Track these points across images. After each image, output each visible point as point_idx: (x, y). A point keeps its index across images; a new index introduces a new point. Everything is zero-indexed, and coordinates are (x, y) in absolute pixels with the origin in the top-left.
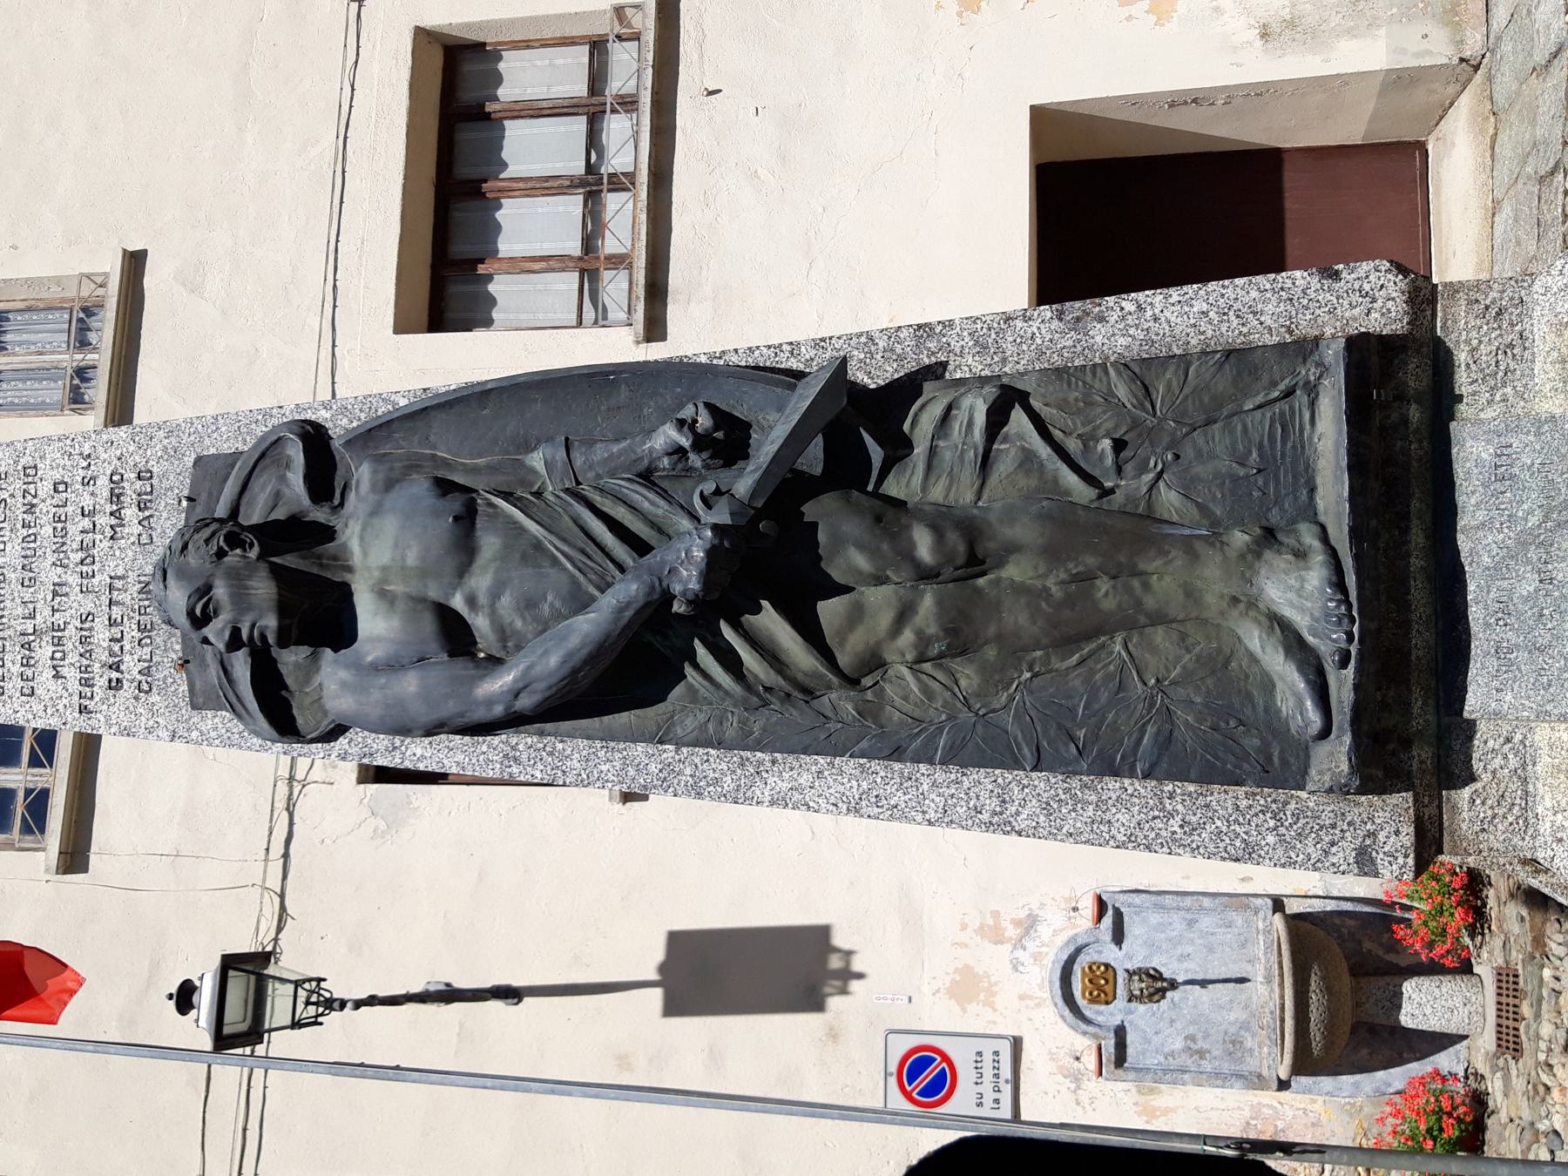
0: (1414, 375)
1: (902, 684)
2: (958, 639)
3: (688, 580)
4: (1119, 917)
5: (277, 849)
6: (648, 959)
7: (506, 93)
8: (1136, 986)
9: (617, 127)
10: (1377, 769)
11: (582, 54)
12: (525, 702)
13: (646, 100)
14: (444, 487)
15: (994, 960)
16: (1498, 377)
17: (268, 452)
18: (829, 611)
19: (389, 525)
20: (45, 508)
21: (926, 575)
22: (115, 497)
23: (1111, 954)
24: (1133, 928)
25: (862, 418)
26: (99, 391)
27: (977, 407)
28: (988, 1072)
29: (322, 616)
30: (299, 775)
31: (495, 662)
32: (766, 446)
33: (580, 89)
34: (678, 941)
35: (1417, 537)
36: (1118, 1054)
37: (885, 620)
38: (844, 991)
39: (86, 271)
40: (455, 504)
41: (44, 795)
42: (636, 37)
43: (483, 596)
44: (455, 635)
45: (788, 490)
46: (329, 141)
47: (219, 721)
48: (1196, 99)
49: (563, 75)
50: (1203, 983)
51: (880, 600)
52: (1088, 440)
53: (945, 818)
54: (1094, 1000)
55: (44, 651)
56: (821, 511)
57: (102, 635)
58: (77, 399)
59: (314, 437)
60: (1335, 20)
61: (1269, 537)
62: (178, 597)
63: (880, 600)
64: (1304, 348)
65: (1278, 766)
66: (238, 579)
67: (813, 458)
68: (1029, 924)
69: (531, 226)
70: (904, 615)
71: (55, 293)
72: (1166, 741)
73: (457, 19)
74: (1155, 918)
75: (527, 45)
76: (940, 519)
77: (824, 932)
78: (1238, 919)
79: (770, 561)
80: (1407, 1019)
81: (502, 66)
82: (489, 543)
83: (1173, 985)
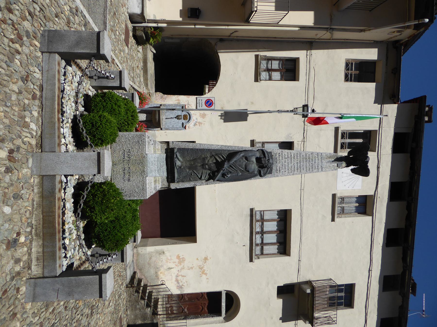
0: (170, 180)
1: (208, 156)
2: (204, 159)
3: (226, 163)
4: (183, 127)
5: (305, 132)
6: (250, 117)
7: (276, 247)
8: (180, 117)
9: (259, 241)
10: (173, 149)
11: (265, 252)
12: (240, 153)
13: (254, 245)
14: (248, 171)
15: (200, 120)
16: (164, 180)
17: (265, 174)
18: (215, 161)
19: (253, 168)
20: (287, 169)
21: (207, 164)
22: (280, 171)
23: (184, 121)
24: (181, 125)
25: (212, 177)
26: (337, 200)
27: (203, 178)
28: (200, 104)
29: (258, 160)
30: (303, 143)
31: (243, 156)
32: (220, 175)
33: (265, 247)
34: (246, 120)
35: (169, 168)
36: (183, 108)
37: (210, 161)
38: (222, 114)
39: (341, 219)
40: (247, 170)
41: (342, 138)
42: (256, 255)
43: (244, 162)
44: (246, 158)
45: (218, 171)
46: (303, 239)
47: (269, 151)
48: (173, 244)
49: (267, 249)
50: (171, 118)
51: (210, 162)
52: (194, 175)
53: (205, 144)
54: (186, 115)
55: (286, 157)
56: (215, 169)
57: (281, 158)
58: (343, 199)
59: (261, 176)
60: (154, 254)
61: (180, 167)
62: (271, 161)
63: (210, 162)
64: (178, 182)
65: (180, 150)
66: (266, 163)
67: (216, 174)
68: (195, 125)
69: (272, 226)
70: (208, 161)
71: (346, 216)
72: (188, 151)
73: (284, 257)
74: (178, 126)
75: (273, 254)
76: (206, 169)
77: (225, 122)
78: (167, 127)
79: (219, 165)
80: (145, 115)
81: (277, 251)
82: (244, 166)
83: (175, 118)
